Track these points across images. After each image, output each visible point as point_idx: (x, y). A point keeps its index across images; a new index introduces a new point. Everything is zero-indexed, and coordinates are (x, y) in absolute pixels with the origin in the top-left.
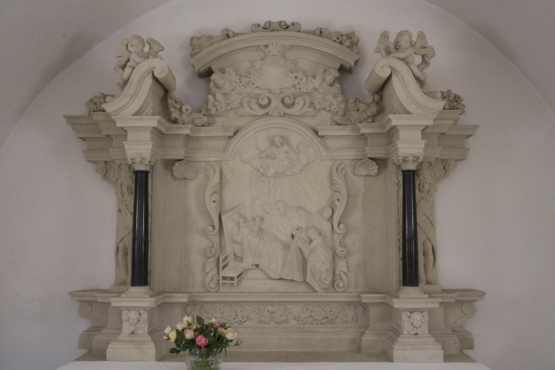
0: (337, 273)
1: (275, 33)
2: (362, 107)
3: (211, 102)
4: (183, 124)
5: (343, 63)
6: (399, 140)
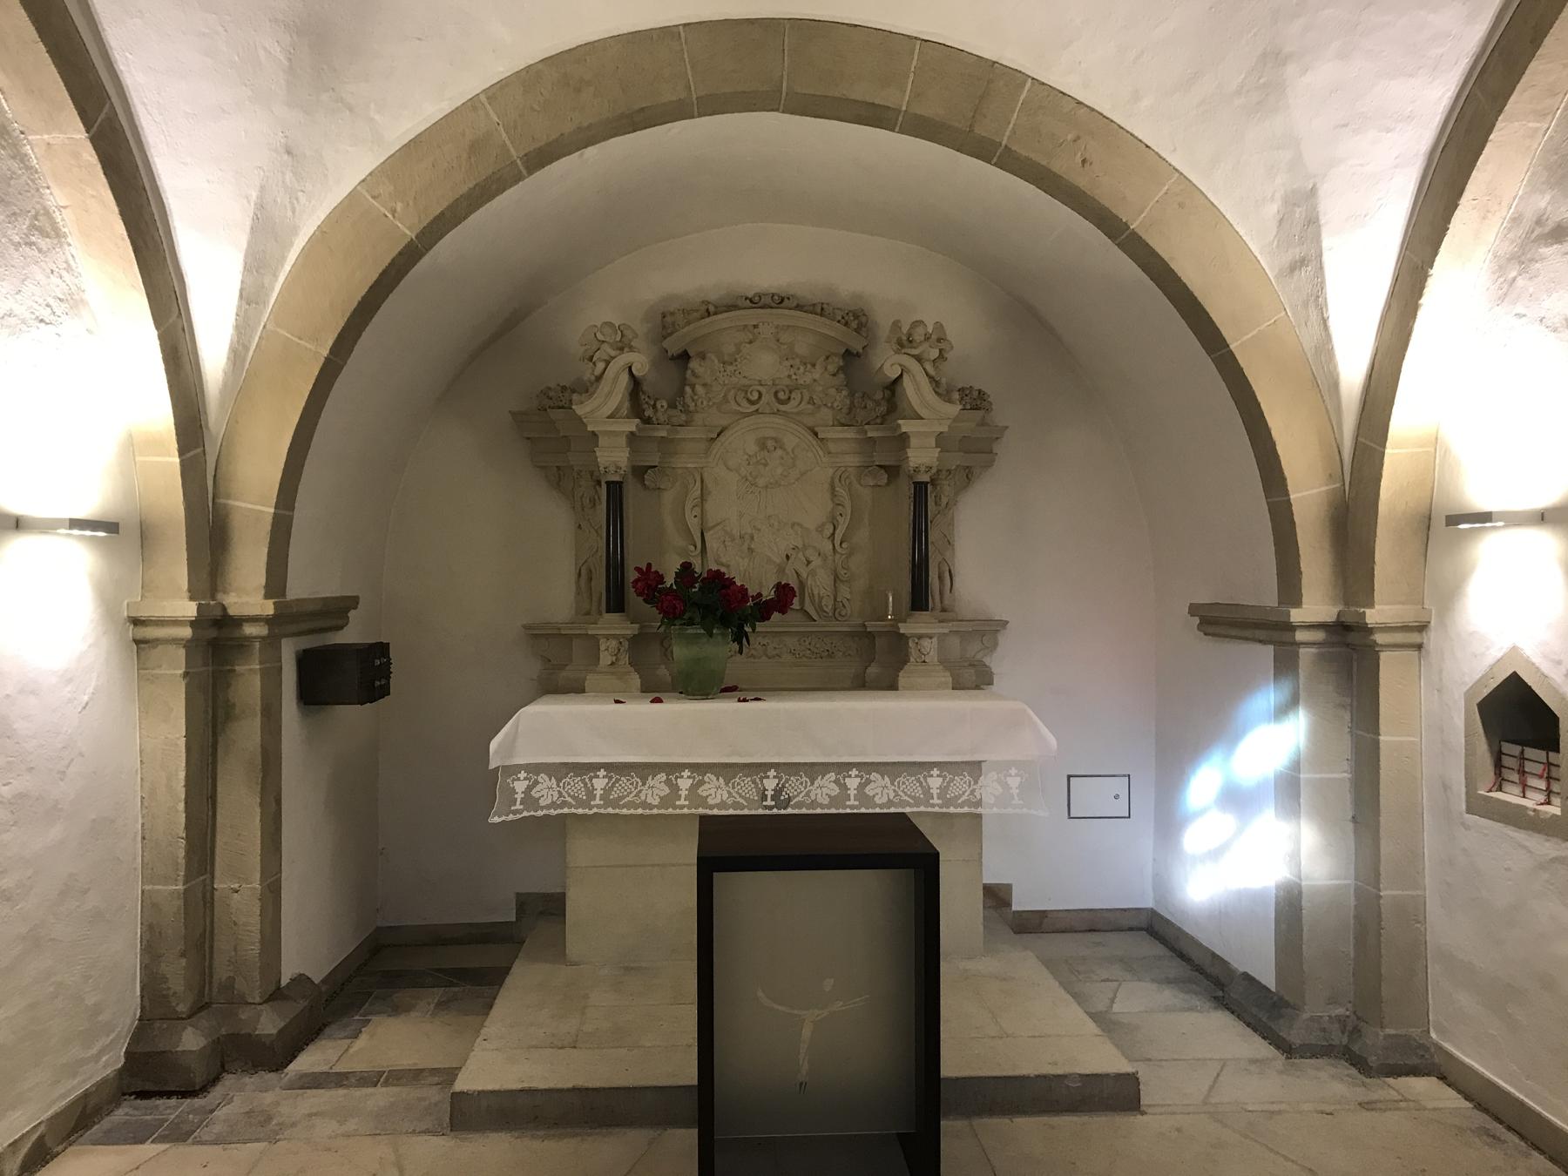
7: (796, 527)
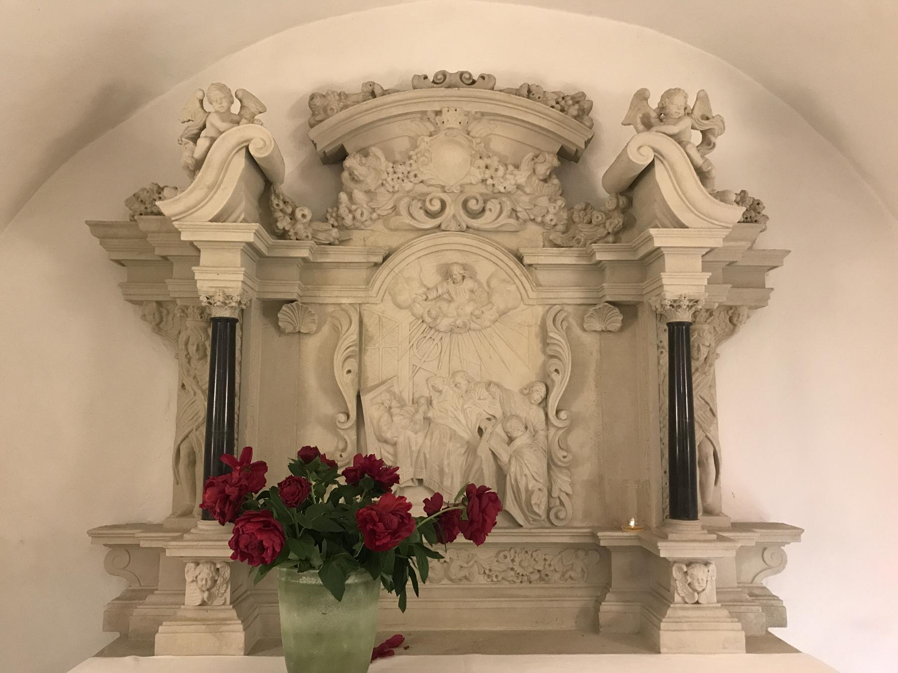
1: (454, 91)
2: (598, 217)
3: (343, 205)
4: (297, 239)
5: (566, 144)
6: (664, 271)
7: (493, 389)
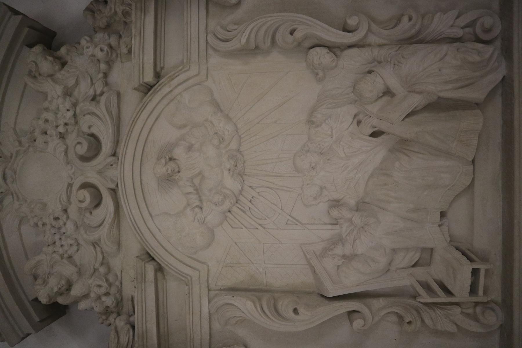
0: (459, 33)
